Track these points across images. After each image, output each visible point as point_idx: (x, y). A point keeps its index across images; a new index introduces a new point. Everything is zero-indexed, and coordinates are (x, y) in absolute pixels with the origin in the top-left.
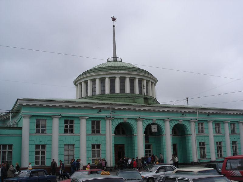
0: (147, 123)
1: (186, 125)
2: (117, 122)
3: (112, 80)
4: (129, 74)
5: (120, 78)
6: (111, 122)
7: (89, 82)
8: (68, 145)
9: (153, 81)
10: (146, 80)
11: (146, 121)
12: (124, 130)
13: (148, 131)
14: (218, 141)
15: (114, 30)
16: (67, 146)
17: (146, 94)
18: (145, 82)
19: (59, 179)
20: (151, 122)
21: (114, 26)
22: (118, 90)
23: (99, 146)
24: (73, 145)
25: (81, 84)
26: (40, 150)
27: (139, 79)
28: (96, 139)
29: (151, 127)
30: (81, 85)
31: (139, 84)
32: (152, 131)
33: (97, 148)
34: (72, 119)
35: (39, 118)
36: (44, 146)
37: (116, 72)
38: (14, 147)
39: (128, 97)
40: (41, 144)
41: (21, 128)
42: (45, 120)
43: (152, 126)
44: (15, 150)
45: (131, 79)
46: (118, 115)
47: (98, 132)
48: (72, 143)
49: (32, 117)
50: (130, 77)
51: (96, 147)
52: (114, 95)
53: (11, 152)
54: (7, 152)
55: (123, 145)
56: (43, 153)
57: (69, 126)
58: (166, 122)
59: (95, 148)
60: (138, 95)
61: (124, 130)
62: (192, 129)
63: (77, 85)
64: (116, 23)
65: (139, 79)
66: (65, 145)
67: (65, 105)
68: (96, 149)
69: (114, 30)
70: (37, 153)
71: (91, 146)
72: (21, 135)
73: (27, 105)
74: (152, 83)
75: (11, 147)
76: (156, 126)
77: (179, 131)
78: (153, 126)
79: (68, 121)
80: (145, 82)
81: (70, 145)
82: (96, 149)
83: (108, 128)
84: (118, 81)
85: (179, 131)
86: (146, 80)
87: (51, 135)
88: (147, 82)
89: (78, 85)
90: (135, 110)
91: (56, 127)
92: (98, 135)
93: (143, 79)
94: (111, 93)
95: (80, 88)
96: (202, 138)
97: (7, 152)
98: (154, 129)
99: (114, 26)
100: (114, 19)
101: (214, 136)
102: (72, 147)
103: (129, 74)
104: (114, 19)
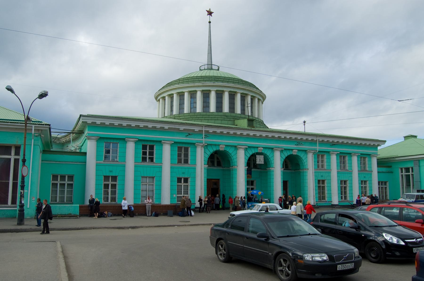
0: (251, 152)
1: (302, 156)
2: (212, 150)
3: (206, 95)
5: (217, 92)
6: (203, 149)
7: (175, 96)
8: (146, 177)
10: (251, 96)
11: (213, 147)
13: (251, 163)
14: (321, 179)
15: (210, 27)
16: (145, 179)
18: (249, 98)
20: (256, 151)
21: (210, 22)
23: (186, 180)
24: (153, 178)
25: (164, 98)
26: (110, 183)
28: (183, 171)
29: (256, 157)
31: (241, 100)
33: (184, 182)
34: (151, 144)
35: (109, 141)
36: (114, 178)
37: (197, 84)
38: (75, 178)
41: (85, 154)
42: (117, 143)
44: (76, 183)
47: (186, 162)
48: (151, 175)
49: (206, 146)
50: (217, 91)
51: (182, 181)
52: (208, 114)
53: (72, 185)
55: (219, 180)
57: (148, 152)
59: (181, 182)
60: (239, 116)
61: (219, 160)
62: (309, 162)
63: (159, 100)
65: (241, 93)
66: (142, 177)
68: (183, 184)
69: (210, 27)
70: (106, 186)
71: (177, 180)
72: (86, 162)
74: (259, 100)
75: (71, 178)
76: (263, 156)
77: (292, 164)
79: (147, 146)
81: (149, 177)
82: (183, 184)
83: (200, 158)
85: (292, 164)
86: (251, 96)
87: (351, 172)
89: (161, 100)
91: (131, 152)
92: (186, 166)
93: (247, 94)
94: (204, 112)
98: (260, 160)
99: (210, 22)
100: (210, 13)
101: (338, 172)
102: (151, 179)
104: (210, 13)
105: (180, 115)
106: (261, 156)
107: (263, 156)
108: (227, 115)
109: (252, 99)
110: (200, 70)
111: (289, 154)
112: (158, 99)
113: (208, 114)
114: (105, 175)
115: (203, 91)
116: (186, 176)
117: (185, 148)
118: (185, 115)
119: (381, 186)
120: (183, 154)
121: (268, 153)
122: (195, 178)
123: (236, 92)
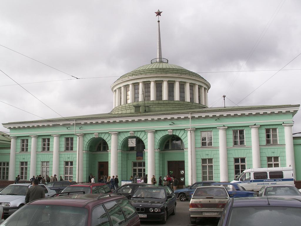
0: (123, 137)
2: (89, 138)
3: (159, 85)
4: (167, 77)
5: (144, 83)
9: (207, 88)
10: (199, 86)
12: (98, 146)
13: (125, 148)
17: (197, 102)
18: (197, 87)
19: (129, 214)
20: (129, 135)
21: (159, 21)
22: (177, 97)
26: (240, 164)
27: (190, 83)
29: (180, 140)
31: (180, 88)
32: (129, 146)
34: (241, 129)
36: (210, 160)
37: (176, 75)
39: (165, 104)
40: (207, 157)
45: (191, 85)
47: (242, 143)
50: (169, 81)
54: (207, 166)
56: (211, 167)
58: (285, 127)
60: (178, 102)
63: (115, 91)
64: (160, 18)
67: (233, 113)
68: (69, 166)
70: (204, 167)
73: (206, 116)
74: (205, 89)
76: (135, 139)
77: (170, 143)
80: (197, 88)
84: (165, 86)
86: (199, 86)
87: (250, 148)
88: (200, 87)
89: (117, 90)
90: (92, 123)
93: (194, 84)
94: (157, 100)
95: (119, 95)
96: (207, 152)
97: (207, 166)
99: (159, 21)
103: (167, 77)
105: (170, 102)
106: (133, 139)
107: (135, 139)
108: (155, 102)
109: (199, 89)
110: (152, 63)
111: (161, 136)
112: (114, 89)
113: (160, 102)
114: (268, 156)
115: (156, 81)
116: (276, 156)
117: (273, 129)
118: (175, 102)
119: (6, 167)
120: (69, 144)
121: (141, 136)
122: (284, 156)
123: (185, 82)
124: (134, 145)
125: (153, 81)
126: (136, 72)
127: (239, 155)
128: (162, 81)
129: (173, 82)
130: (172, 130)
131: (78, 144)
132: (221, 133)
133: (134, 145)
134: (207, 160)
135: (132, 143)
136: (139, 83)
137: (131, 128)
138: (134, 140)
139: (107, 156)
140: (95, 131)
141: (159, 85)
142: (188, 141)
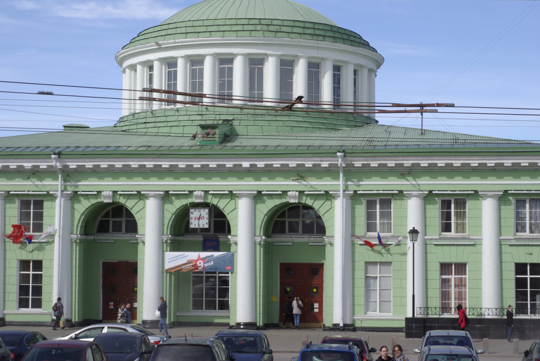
3: (255, 65)
12: (110, 221)
30: (151, 68)
36: (461, 268)
40: (453, 260)
43: (192, 210)
46: (265, 184)
76: (207, 211)
78: (194, 214)
84: (239, 68)
89: (139, 67)
98: (200, 220)
107: (207, 211)
121: (221, 204)
124: (204, 223)
125: (243, 55)
126: (195, 24)
127: (453, 256)
128: (266, 55)
129: (293, 59)
130: (297, 193)
131: (56, 217)
132: (488, 207)
133: (204, 223)
134: (453, 266)
135: (200, 220)
136: (203, 57)
137: (198, 186)
138: (205, 213)
139: (134, 246)
140: (106, 188)
141: (255, 65)
142: (336, 217)
